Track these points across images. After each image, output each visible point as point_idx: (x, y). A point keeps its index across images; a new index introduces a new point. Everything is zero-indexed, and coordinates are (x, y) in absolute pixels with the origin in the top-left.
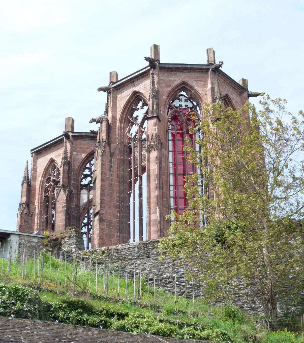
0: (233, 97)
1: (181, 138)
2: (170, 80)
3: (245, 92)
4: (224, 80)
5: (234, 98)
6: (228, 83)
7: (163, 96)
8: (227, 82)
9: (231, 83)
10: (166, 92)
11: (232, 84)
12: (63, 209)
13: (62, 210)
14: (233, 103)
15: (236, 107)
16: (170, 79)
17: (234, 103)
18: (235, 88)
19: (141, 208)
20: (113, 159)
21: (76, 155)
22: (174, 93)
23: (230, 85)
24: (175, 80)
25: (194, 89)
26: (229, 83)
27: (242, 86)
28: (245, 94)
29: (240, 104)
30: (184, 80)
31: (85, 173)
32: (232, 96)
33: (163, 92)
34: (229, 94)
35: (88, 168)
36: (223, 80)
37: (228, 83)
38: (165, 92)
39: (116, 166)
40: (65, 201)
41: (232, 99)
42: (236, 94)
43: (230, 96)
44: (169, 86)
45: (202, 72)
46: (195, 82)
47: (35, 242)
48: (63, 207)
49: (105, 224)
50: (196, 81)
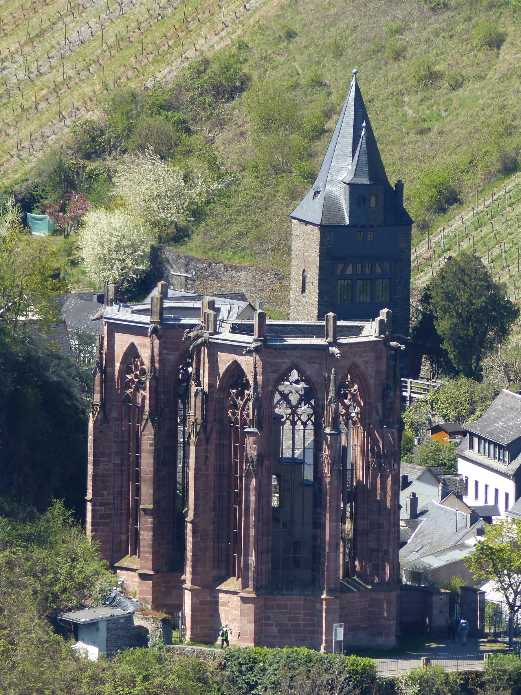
1: (291, 427)
12: (150, 448)
13: (149, 450)
16: (278, 361)
19: (301, 328)
20: (208, 447)
21: (167, 354)
24: (284, 363)
39: (213, 455)
40: (152, 437)
46: (308, 365)
47: (122, 623)
48: (150, 445)
50: (310, 363)
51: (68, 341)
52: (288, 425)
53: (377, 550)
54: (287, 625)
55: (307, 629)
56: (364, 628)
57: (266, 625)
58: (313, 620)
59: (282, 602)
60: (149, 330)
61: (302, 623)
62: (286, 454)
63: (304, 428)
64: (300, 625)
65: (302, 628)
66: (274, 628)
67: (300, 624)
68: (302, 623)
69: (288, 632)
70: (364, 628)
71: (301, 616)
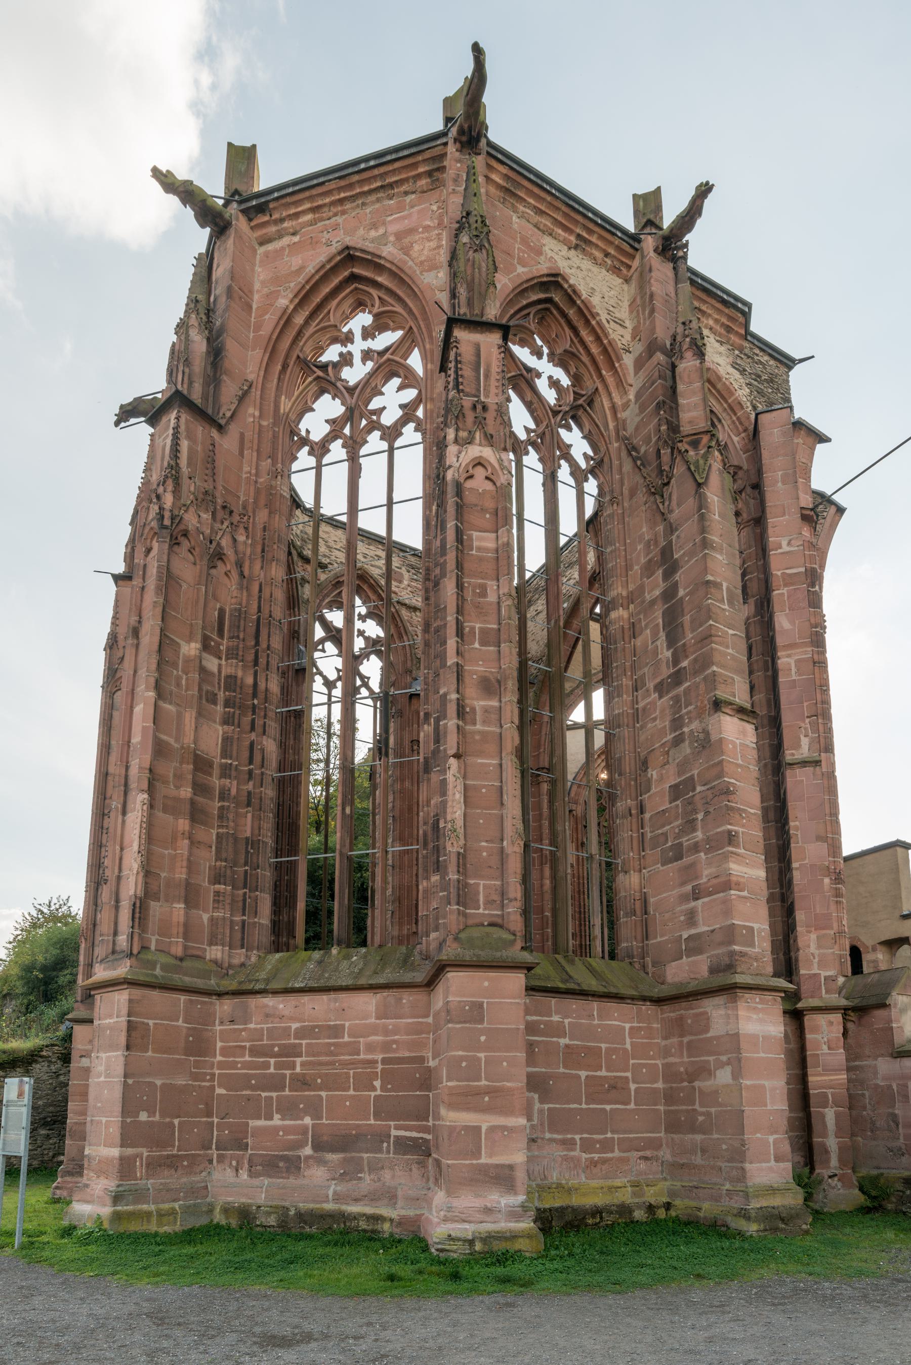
1: (385, 445)
4: (313, 210)
6: (341, 201)
8: (333, 203)
9: (351, 186)
11: (361, 182)
26: (342, 195)
30: (349, 241)
36: (309, 217)
52: (532, 459)
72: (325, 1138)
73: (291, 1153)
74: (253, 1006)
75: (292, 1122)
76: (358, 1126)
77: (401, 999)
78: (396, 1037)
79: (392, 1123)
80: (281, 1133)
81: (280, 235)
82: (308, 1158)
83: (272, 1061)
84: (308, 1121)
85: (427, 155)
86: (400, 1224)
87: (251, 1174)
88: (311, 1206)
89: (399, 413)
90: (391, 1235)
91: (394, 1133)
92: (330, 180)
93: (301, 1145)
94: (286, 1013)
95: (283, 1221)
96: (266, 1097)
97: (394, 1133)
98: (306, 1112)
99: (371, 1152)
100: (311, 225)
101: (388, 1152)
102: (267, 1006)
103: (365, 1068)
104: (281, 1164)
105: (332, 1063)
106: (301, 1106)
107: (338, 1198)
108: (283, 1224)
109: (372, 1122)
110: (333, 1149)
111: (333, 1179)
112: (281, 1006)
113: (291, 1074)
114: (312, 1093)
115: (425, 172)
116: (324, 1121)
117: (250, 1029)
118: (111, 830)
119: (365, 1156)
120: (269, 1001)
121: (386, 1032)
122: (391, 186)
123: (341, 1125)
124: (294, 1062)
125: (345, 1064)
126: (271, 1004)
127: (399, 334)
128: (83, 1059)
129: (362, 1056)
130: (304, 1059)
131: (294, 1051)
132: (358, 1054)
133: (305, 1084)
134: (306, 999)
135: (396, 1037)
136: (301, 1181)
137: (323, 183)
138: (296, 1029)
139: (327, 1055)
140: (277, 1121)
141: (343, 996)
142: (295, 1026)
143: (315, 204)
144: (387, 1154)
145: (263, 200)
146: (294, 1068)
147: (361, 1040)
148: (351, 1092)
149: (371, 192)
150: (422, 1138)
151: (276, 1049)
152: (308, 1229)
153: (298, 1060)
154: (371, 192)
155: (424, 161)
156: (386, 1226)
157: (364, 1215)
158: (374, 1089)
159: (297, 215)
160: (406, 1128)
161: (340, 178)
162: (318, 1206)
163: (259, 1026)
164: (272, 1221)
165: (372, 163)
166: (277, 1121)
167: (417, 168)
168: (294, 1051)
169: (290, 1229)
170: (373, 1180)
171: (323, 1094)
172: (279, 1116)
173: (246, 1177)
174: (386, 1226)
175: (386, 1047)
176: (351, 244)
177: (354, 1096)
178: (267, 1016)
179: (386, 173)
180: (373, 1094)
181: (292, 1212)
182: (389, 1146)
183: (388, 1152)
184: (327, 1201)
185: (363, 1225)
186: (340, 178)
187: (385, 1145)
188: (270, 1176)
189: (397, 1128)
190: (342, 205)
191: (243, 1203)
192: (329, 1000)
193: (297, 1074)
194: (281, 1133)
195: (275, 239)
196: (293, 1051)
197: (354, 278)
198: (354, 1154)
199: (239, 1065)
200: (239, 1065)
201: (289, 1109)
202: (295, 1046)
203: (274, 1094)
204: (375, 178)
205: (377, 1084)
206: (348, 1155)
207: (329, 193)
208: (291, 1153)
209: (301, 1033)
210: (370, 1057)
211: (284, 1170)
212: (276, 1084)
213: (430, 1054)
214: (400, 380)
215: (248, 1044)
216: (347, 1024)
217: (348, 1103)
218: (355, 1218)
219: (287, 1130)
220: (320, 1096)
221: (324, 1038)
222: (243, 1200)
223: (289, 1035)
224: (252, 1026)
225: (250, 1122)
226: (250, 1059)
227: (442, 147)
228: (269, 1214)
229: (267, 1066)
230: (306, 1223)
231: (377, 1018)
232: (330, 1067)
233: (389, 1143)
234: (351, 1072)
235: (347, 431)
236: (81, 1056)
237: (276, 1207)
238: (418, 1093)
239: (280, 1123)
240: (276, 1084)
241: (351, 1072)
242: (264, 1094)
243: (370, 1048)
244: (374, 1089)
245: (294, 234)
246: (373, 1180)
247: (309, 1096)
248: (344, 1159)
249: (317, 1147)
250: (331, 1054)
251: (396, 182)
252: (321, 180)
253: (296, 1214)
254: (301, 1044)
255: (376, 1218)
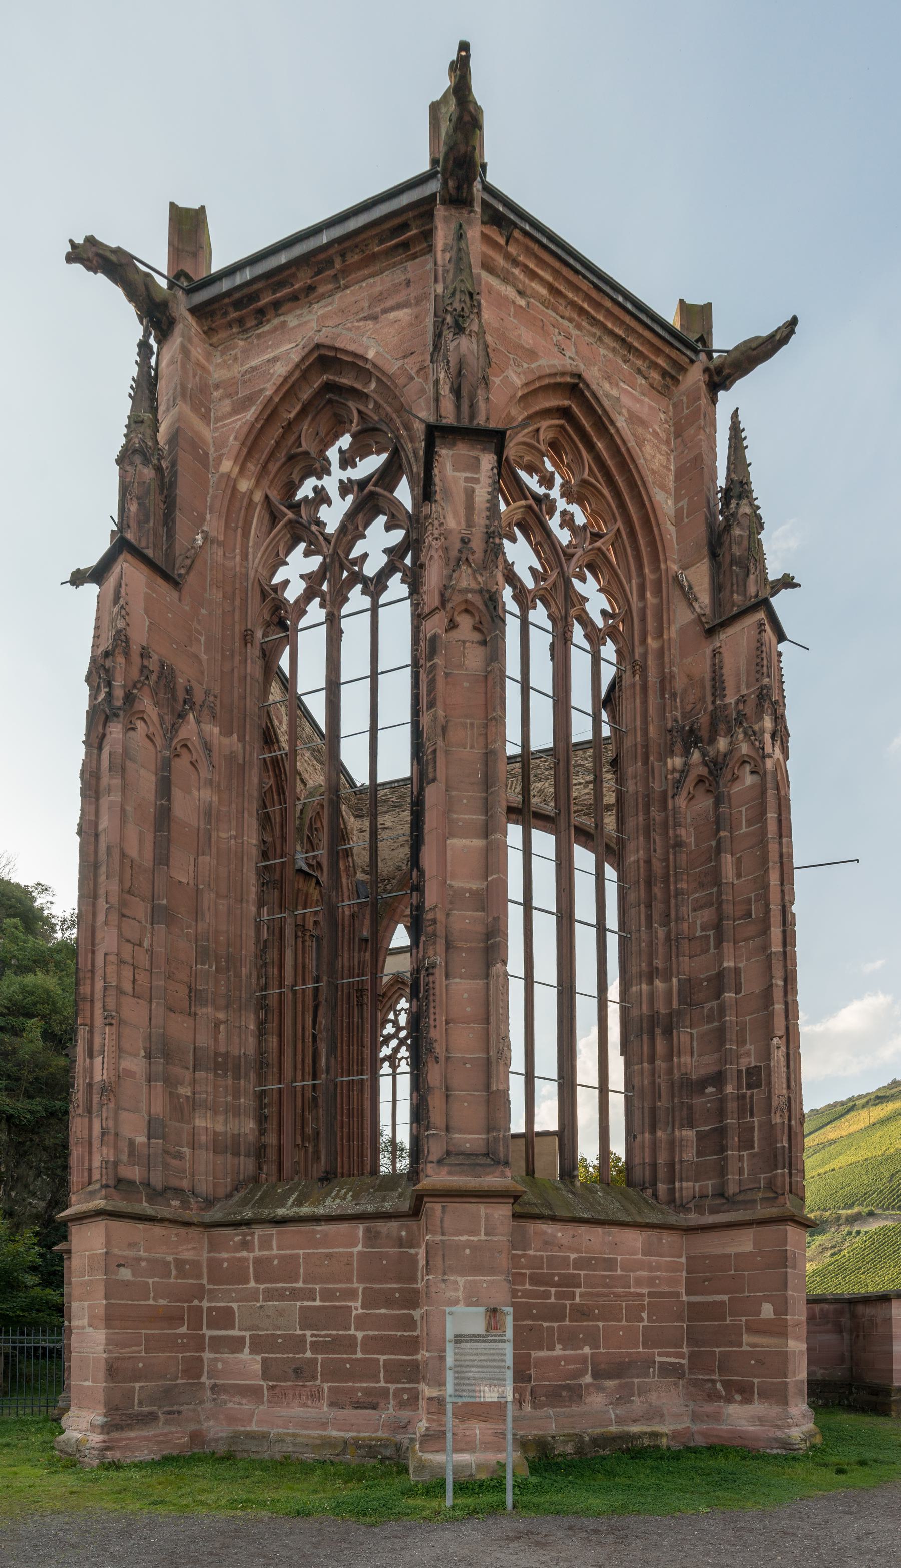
0: (614, 392)
2: (253, 369)
3: (692, 362)
4: (552, 289)
5: (625, 400)
6: (581, 311)
7: (219, 461)
8: (572, 304)
9: (598, 306)
10: (236, 439)
11: (609, 313)
14: (612, 423)
15: (632, 444)
16: (253, 363)
17: (621, 423)
18: (629, 339)
22: (283, 437)
23: (594, 321)
25: (370, 374)
26: (585, 306)
27: (678, 326)
28: (695, 376)
29: (663, 436)
31: (385, 1032)
32: (606, 386)
33: (220, 444)
34: (586, 375)
35: (390, 1021)
36: (543, 291)
37: (581, 311)
38: (231, 439)
41: (606, 403)
42: (641, 381)
43: (594, 387)
44: (248, 401)
45: (405, 245)
46: (370, 324)
49: (700, 1186)
51: (568, 585)
53: (718, 1078)
54: (298, 1344)
55: (382, 1358)
56: (667, 1370)
57: (217, 1344)
58: (410, 1323)
59: (275, 1252)
60: (286, 519)
61: (360, 1335)
62: (406, 959)
63: (394, 1071)
64: (350, 1344)
65: (359, 1355)
66: (246, 1355)
67: (354, 1337)
68: (360, 1335)
69: (301, 1372)
70: (667, 1370)
71: (357, 1307)
72: (603, 1366)
73: (572, 1382)
74: (531, 1232)
75: (573, 1352)
76: (631, 1353)
77: (661, 1239)
78: (659, 1273)
79: (656, 1351)
80: (563, 1363)
81: (506, 279)
82: (588, 1386)
83: (553, 1290)
84: (587, 1350)
85: (674, 354)
86: (674, 1437)
87: (535, 1406)
88: (599, 1430)
89: (384, 559)
90: (668, 1449)
91: (658, 1359)
92: (585, 277)
93: (581, 1373)
94: (565, 1241)
95: (579, 1448)
96: (547, 1327)
97: (658, 1359)
98: (585, 1342)
99: (641, 1377)
100: (542, 303)
101: (654, 1377)
102: (545, 1233)
103: (635, 1301)
104: (564, 1394)
105: (607, 1295)
106: (581, 1336)
107: (620, 1421)
108: (579, 1451)
109: (641, 1350)
110: (610, 1377)
111: (611, 1404)
112: (559, 1234)
113: (571, 1305)
114: (591, 1323)
115: (663, 369)
116: (601, 1350)
117: (530, 1256)
118: (438, 993)
119: (636, 1380)
120: (548, 1228)
121: (651, 1269)
122: (630, 348)
123: (616, 1353)
124: (574, 1292)
125: (618, 1296)
126: (549, 1231)
127: (385, 456)
128: (122, 1269)
129: (632, 1290)
130: (583, 1289)
131: (573, 1281)
132: (630, 1288)
133: (584, 1314)
134: (582, 1229)
135: (659, 1273)
136: (583, 1409)
137: (577, 272)
138: (574, 1259)
139: (604, 1287)
140: (558, 1351)
141: (615, 1230)
142: (573, 1256)
143: (556, 285)
144: (653, 1379)
145: (512, 217)
146: (574, 1299)
147: (631, 1274)
148: (624, 1323)
149: (611, 333)
150: (679, 1363)
151: (556, 1278)
152: (601, 1452)
153: (578, 1291)
154: (611, 333)
155: (668, 357)
156: (664, 1441)
157: (646, 1433)
158: (642, 1320)
159: (533, 275)
160: (667, 1355)
161: (596, 287)
162: (605, 1430)
163: (538, 1253)
164: (569, 1449)
165: (629, 306)
166: (558, 1351)
167: (658, 356)
168: (573, 1281)
169: (586, 1454)
170: (642, 1402)
171: (600, 1324)
172: (561, 1347)
173: (529, 1409)
174: (664, 1441)
175: (651, 1281)
176: (584, 375)
177: (627, 1326)
178: (546, 1243)
179: (633, 331)
180: (641, 1324)
181: (587, 1439)
182: (654, 1371)
183: (654, 1377)
184: (611, 1425)
185: (646, 1442)
186: (596, 287)
187: (651, 1370)
188: (554, 1407)
189: (659, 1355)
190: (579, 315)
191: (536, 1436)
192: (604, 1233)
193: (577, 1304)
194: (563, 1363)
195: (498, 276)
196: (571, 1281)
197: (565, 413)
198: (627, 1380)
199: (519, 1294)
200: (519, 1294)
201: (569, 1339)
202: (573, 1276)
203: (555, 1325)
204: (622, 323)
205: (645, 1315)
206: (623, 1381)
207: (576, 289)
208: (572, 1382)
209: (579, 1264)
210: (638, 1290)
211: (567, 1399)
212: (556, 1314)
213: (684, 1290)
214: (386, 518)
215: (528, 1272)
216: (619, 1258)
217: (621, 1333)
218: (640, 1437)
219: (566, 1359)
220: (597, 1326)
221: (600, 1271)
222: (535, 1432)
223: (568, 1265)
224: (531, 1252)
225: (532, 1352)
226: (531, 1288)
227: (687, 360)
228: (566, 1443)
229: (547, 1295)
230: (599, 1447)
231: (643, 1255)
232: (606, 1299)
233: (654, 1368)
234: (624, 1304)
235: (408, 561)
236: (119, 1266)
237: (568, 1435)
238: (383, 1311)
239: (561, 1353)
240: (556, 1314)
241: (624, 1304)
242: (545, 1324)
243: (639, 1282)
244: (642, 1320)
245: (520, 293)
246: (642, 1402)
247: (588, 1326)
248: (620, 1385)
249: (596, 1375)
250: (606, 1286)
251: (637, 350)
252: (578, 267)
253: (590, 1440)
254: (298, 1255)
255: (655, 1435)
